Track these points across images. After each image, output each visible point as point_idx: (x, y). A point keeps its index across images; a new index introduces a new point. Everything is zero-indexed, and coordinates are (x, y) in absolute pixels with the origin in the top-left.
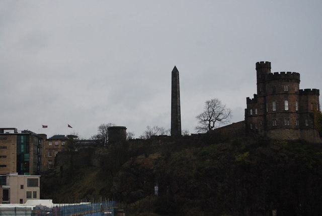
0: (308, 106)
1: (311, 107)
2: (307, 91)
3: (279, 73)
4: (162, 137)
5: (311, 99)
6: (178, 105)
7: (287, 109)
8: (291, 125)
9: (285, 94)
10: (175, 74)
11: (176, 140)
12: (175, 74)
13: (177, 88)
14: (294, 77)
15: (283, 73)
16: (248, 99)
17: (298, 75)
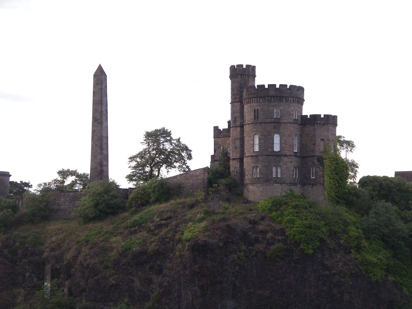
0: (315, 144)
1: (320, 146)
2: (315, 118)
3: (267, 87)
4: (344, 168)
5: (320, 132)
6: (104, 135)
7: (277, 148)
8: (284, 176)
9: (275, 123)
10: (100, 77)
11: (95, 198)
12: (100, 77)
13: (102, 104)
14: (294, 94)
15: (272, 86)
16: (216, 128)
17: (301, 90)
